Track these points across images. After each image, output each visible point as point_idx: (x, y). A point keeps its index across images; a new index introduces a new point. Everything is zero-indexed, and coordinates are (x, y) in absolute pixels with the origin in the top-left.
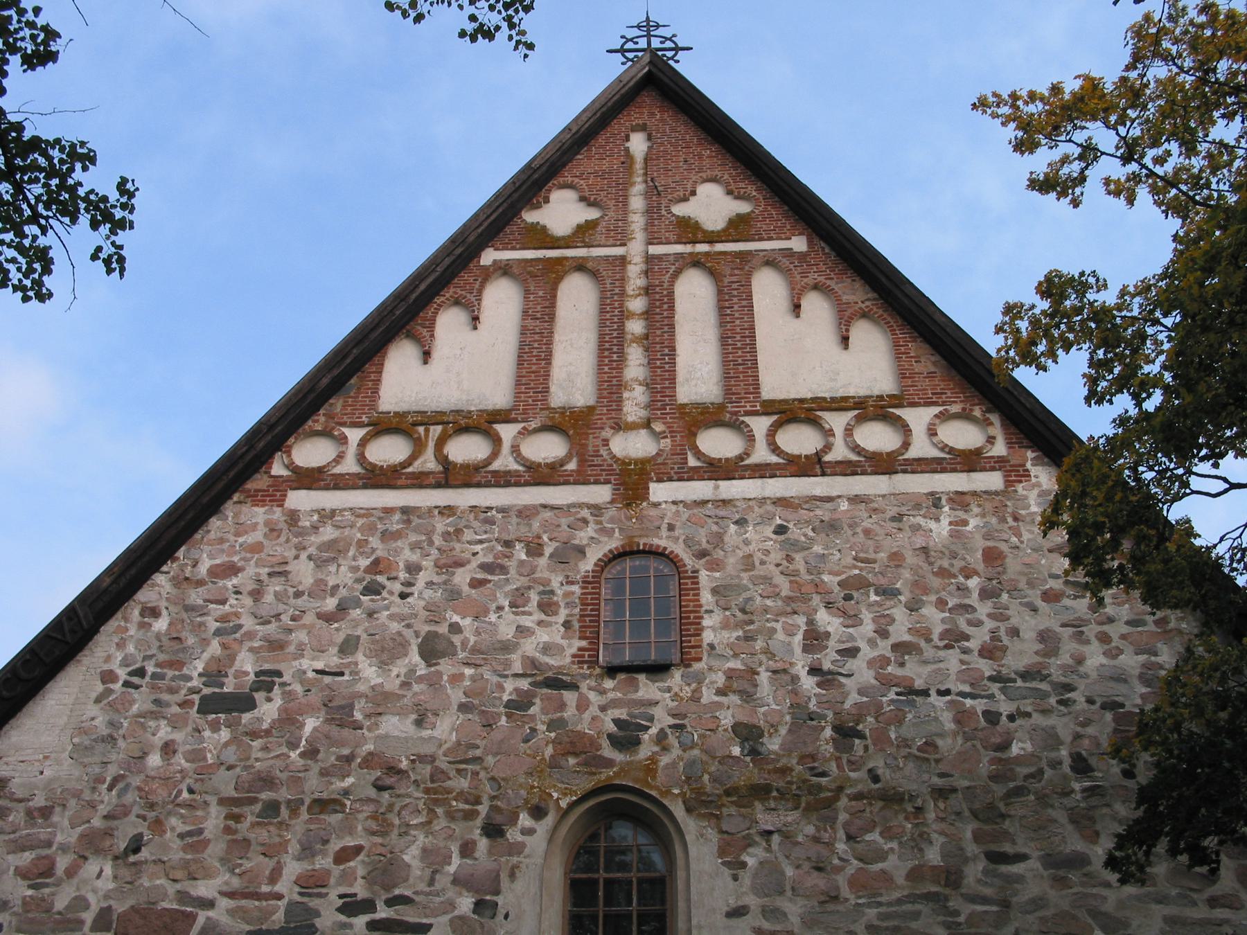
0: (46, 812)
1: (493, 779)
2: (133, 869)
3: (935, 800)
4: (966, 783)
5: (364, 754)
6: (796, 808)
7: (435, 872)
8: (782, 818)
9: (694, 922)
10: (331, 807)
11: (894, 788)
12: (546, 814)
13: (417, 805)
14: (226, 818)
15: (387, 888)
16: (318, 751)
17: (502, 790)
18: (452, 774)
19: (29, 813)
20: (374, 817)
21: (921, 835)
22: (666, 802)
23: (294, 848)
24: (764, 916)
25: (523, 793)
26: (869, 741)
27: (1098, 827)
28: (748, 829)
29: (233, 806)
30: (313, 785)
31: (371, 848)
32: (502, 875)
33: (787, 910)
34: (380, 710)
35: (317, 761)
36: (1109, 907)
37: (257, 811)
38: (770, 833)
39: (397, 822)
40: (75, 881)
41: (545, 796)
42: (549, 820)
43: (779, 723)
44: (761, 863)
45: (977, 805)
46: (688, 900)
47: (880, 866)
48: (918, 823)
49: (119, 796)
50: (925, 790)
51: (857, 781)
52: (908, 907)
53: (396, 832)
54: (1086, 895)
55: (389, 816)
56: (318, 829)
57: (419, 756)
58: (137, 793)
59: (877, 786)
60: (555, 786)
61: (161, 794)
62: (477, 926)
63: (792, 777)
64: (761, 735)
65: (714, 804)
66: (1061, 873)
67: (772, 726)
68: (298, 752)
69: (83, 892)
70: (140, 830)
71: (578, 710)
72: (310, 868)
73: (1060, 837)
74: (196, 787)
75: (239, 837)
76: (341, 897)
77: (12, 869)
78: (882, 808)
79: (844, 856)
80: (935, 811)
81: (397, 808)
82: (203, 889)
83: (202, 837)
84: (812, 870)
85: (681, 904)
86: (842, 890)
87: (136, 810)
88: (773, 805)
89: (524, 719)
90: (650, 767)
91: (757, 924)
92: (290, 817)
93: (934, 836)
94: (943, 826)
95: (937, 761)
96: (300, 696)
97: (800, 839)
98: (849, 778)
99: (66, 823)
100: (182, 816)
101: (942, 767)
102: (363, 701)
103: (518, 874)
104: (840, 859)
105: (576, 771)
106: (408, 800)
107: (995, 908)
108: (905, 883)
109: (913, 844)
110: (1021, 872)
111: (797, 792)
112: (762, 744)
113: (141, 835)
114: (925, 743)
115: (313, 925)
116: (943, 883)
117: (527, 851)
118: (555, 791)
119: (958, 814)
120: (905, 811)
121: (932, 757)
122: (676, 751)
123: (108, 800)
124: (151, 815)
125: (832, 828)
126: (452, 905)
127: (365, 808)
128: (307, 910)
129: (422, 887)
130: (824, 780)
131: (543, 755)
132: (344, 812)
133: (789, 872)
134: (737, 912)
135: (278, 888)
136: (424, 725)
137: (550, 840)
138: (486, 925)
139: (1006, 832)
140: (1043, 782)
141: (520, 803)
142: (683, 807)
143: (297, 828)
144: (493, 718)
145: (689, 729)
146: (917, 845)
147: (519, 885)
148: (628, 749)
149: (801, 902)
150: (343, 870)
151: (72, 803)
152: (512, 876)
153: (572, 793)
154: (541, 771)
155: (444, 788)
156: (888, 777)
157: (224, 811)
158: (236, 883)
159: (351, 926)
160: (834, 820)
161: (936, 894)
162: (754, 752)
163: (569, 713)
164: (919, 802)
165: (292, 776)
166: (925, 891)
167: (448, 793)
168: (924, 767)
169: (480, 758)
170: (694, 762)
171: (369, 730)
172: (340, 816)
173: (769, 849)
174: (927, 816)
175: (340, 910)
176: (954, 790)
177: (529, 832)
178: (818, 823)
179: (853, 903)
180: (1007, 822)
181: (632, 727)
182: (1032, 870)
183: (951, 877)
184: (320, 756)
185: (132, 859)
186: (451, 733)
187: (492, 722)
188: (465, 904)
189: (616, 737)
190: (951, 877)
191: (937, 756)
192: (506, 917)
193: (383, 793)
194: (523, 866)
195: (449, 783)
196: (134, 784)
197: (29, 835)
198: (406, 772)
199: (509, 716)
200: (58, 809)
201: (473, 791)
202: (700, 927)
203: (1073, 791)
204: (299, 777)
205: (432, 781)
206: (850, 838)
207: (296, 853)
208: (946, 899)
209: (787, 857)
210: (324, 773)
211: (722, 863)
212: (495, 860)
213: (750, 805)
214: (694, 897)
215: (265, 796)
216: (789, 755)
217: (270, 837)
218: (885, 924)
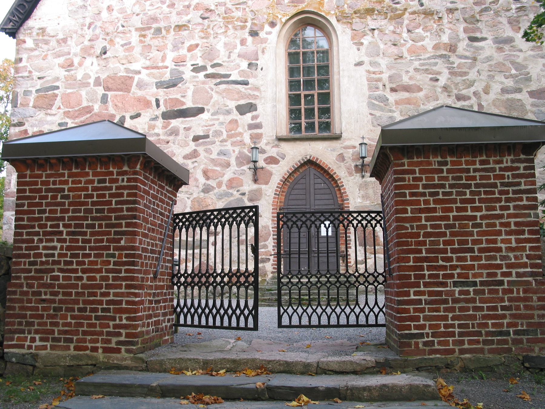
0: (65, 40)
1: (252, 11)
2: (105, 61)
3: (448, 14)
4: (463, 6)
6: (386, 18)
9: (341, 68)
10: (183, 28)
12: (276, 25)
14: (140, 36)
15: (211, 60)
16: (175, 4)
18: (234, 10)
19: (58, 41)
20: (202, 31)
21: (440, 30)
23: (170, 46)
25: (266, 16)
27: (520, 25)
29: (142, 31)
30: (175, 20)
32: (259, 52)
33: (380, 63)
36: (519, 60)
37: (152, 32)
38: (374, 30)
39: (212, 32)
40: (83, 67)
41: (275, 17)
42: (278, 27)
44: (370, 43)
45: (467, 16)
47: (421, 43)
49: (93, 31)
50: (444, 10)
51: (413, 6)
52: (433, 61)
53: (212, 36)
54: (510, 55)
55: (208, 30)
57: (219, 3)
58: (100, 29)
60: (279, 13)
61: (110, 29)
66: (501, 46)
69: (87, 72)
70: (105, 45)
73: (502, 30)
74: (125, 24)
75: (146, 44)
76: (192, 65)
77: (57, 64)
78: (424, 18)
79: (406, 39)
82: (135, 66)
83: (131, 45)
85: (335, 61)
87: (102, 36)
88: (375, 18)
91: (367, 69)
93: (446, 30)
94: (451, 25)
97: (387, 32)
99: (74, 44)
100: (121, 37)
104: (404, 40)
106: (216, 23)
107: (470, 61)
108: (432, 50)
110: (483, 45)
111: (386, 11)
113: (106, 47)
115: (182, 78)
116: (448, 50)
117: (269, 41)
119: (458, 20)
120: (434, 19)
123: (89, 33)
124: (108, 38)
125: (401, 27)
126: (239, 66)
127: (198, 27)
129: (226, 59)
130: (398, 6)
133: (382, 46)
135: (166, 64)
137: (279, 36)
139: (479, 28)
140: (498, 5)
141: (265, 20)
142: (336, 19)
143: (170, 38)
147: (266, 56)
149: (387, 59)
151: (74, 36)
152: (263, 52)
153: (287, 15)
154: (273, 6)
156: (427, 4)
157: (138, 33)
158: (148, 63)
159: (198, 77)
160: (402, 23)
161: (445, 55)
164: (440, 15)
167: (233, 18)
172: (187, 32)
173: (373, 37)
174: (444, 21)
176: (457, 9)
177: (270, 33)
180: (479, 24)
182: (488, 44)
183: (452, 48)
184: (176, 6)
185: (104, 56)
188: (244, 65)
190: (452, 48)
192: (262, 69)
194: (267, 48)
195: (233, 14)
196: (98, 26)
197: (60, 50)
200: (69, 39)
203: (511, 9)
205: (226, 14)
206: (409, 31)
208: (449, 57)
210: (178, 14)
213: (366, 18)
214: (341, 58)
215: (155, 26)
217: (159, 43)
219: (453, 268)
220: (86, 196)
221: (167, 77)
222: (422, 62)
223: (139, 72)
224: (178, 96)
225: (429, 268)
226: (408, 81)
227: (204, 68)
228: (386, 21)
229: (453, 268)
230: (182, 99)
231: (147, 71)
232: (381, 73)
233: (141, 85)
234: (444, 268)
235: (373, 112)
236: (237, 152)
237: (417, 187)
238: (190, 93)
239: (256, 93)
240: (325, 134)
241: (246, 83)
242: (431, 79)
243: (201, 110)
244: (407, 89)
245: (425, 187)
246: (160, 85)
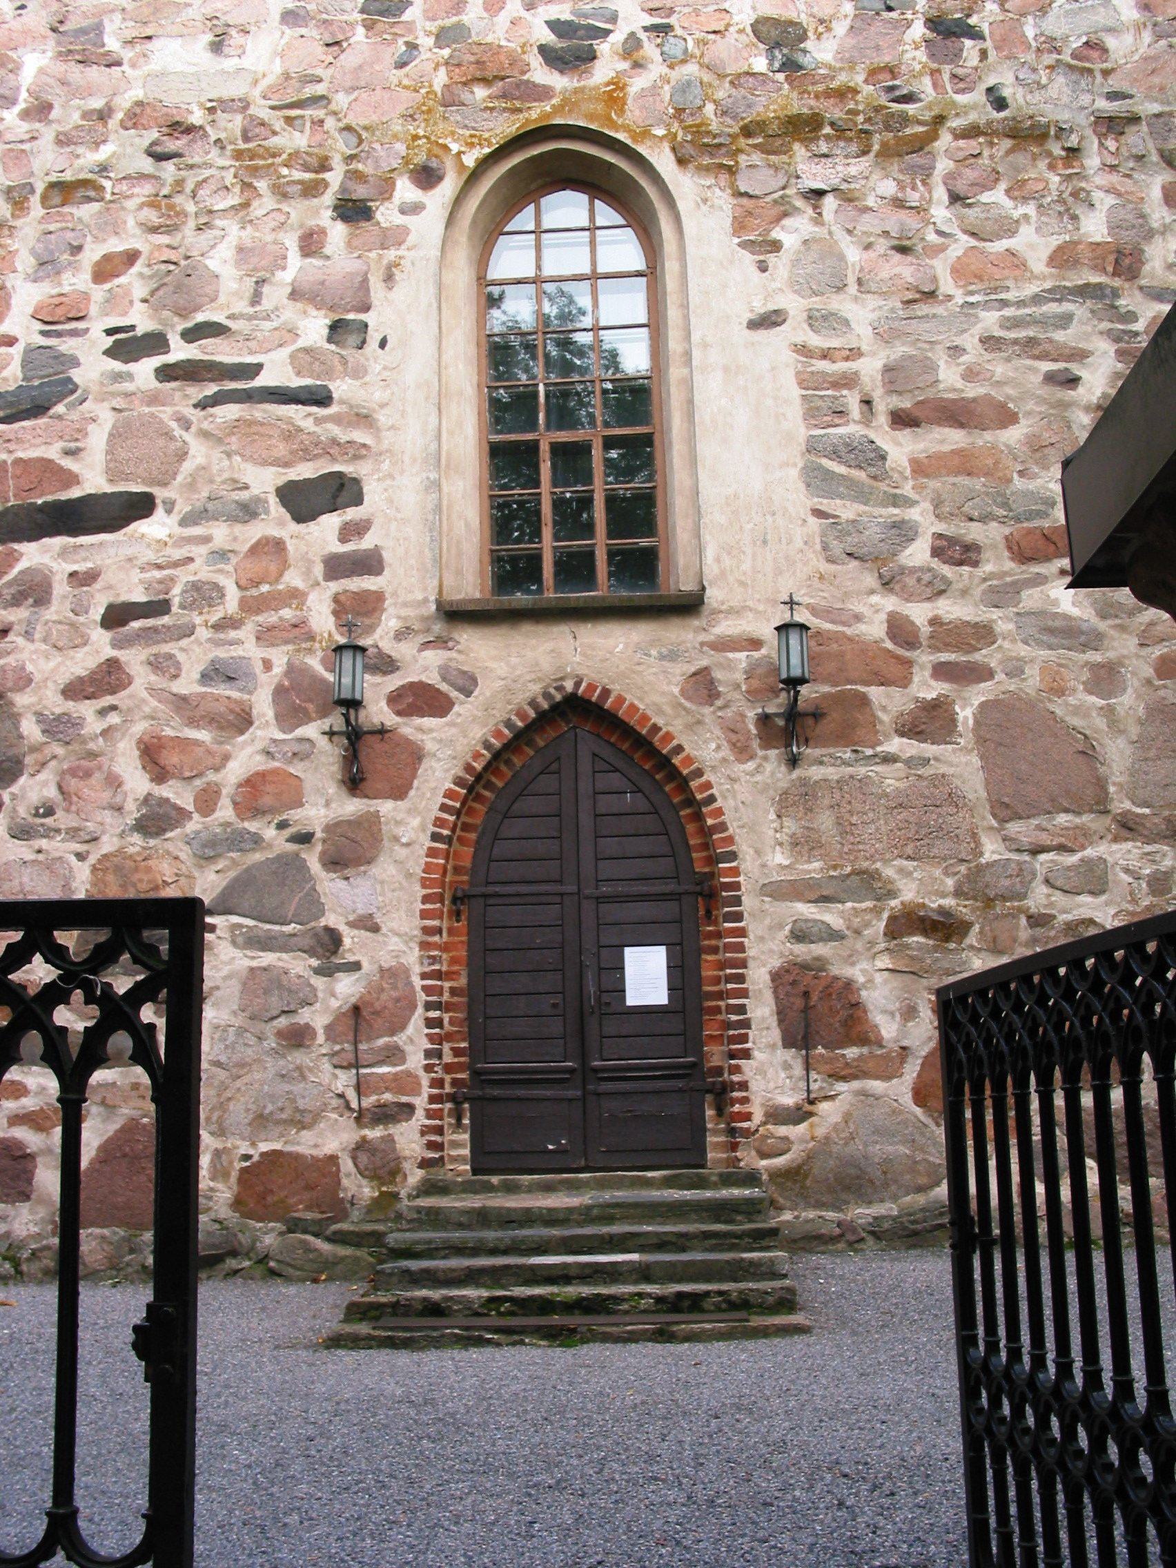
1: (348, 128)
3: (1101, 137)
4: (1156, 108)
5: (127, 105)
6: (865, 153)
7: (261, 282)
8: (839, 168)
9: (696, 337)
10: (81, 192)
11: (1031, 117)
12: (440, 179)
13: (223, 178)
15: (183, 313)
16: (50, 107)
17: (365, 146)
18: (278, 125)
20: (153, 204)
21: (1075, 195)
22: (641, 149)
24: (810, 325)
25: (400, 148)
26: (988, 44)
28: (784, 188)
31: (151, 253)
33: (849, 316)
34: (149, 32)
35: (51, 122)
38: (820, 193)
39: (191, 208)
41: (436, 150)
42: (448, 187)
43: (833, 17)
44: (805, 242)
46: (685, 306)
48: (1070, 176)
50: (1084, 120)
51: (966, 109)
52: (1052, 308)
53: (192, 223)
55: (178, 199)
56: (62, 229)
59: (1002, 114)
60: (453, 133)
62: (336, 360)
63: (857, 103)
64: (803, 37)
65: (724, 150)
67: (822, 21)
68: (17, 109)
71: (486, 10)
72: (55, 291)
76: (110, 332)
78: (1009, 152)
80: (1100, 153)
81: (189, 186)
84: (893, 252)
86: (941, 282)
89: (394, 30)
90: (614, 96)
92: (13, 215)
93: (1097, 195)
94: (1114, 178)
95: (1106, 73)
96: (9, 17)
97: (871, 202)
98: (954, 104)
101: (1114, 83)
102: (118, 17)
103: (398, 276)
104: (940, 233)
105: (487, 108)
106: (207, 173)
109: (1062, 209)
111: (866, 127)
112: (805, 51)
114: (1086, 43)
115: (70, 380)
116: (1110, 269)
117: (411, 239)
118: (455, 141)
119: (1140, 158)
120: (1049, 154)
121: (1098, 67)
122: (657, 69)
125: (924, 182)
126: (293, 332)
127: (136, 190)
128: (56, 358)
129: (242, 306)
130: (910, 108)
131: (431, 86)
132: (102, 199)
133: (853, 255)
134: (768, 321)
136: (226, 50)
137: (451, 221)
138: (351, 359)
143: (27, 230)
144: (343, 31)
145: (679, 32)
146: (1068, 210)
147: (401, 292)
148: (577, 67)
149: (873, 301)
150: (109, 291)
152: (389, 278)
154: (429, 111)
155: (267, 149)
156: (1021, 101)
159: (130, 377)
161: (1099, 286)
162: (791, 66)
163: (472, 15)
164: (1073, 141)
165: (11, 150)
166: (1080, 282)
168: (1083, 84)
169: (323, 97)
170: (689, 83)
171: (133, 65)
172: (96, 206)
173: (818, 219)
175: (110, 353)
176: (1135, 119)
177: (414, 209)
178: (901, 177)
179: (961, 302)
181: (581, 33)
184: (54, 114)
186: (272, 62)
187: (340, 37)
188: (314, 328)
189: (553, 50)
191: (1105, 65)
192: (383, 344)
193: (164, 163)
195: (274, 141)
198: (201, 127)
199: (369, 26)
201: (316, 150)
202: (705, 346)
204: (23, 151)
205: (246, 139)
206: (956, 198)
207: (30, 271)
208: (1116, 294)
209: (849, 232)
211: (739, 245)
212: (359, 257)
213: (787, 151)
216: (852, 69)
218: (1012, 335)
222: (1009, 312)
224: (53, 452)
227: (156, 342)
230: (67, 463)
232: (854, 354)
235: (825, 504)
236: (278, 670)
238: (97, 440)
239: (359, 436)
241: (320, 398)
242: (1050, 378)
243: (141, 506)
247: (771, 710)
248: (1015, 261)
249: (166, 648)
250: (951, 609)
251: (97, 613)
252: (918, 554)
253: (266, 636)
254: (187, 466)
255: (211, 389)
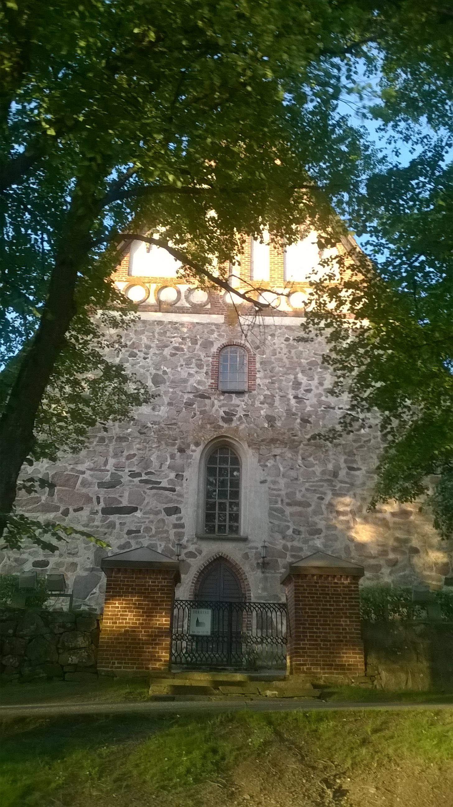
23: (111, 453)
42: (201, 448)
82: (80, 467)
90: (236, 430)
134: (263, 482)
135: (108, 467)
149: (285, 479)
162: (272, 426)
173: (275, 461)
183: (335, 474)
188: (172, 475)
208: (333, 481)
219: (321, 633)
220: (145, 589)
221: (107, 478)
222: (311, 484)
223: (84, 473)
224: (117, 496)
225: (310, 632)
226: (300, 498)
227: (139, 475)
228: (287, 449)
229: (321, 633)
230: (119, 499)
231: (92, 473)
232: (280, 490)
233: (85, 484)
234: (316, 633)
235: (272, 521)
236: (162, 547)
237: (304, 593)
238: (126, 494)
239: (180, 499)
240: (234, 536)
241: (173, 490)
242: (319, 498)
243: (135, 509)
244: (299, 504)
245: (308, 593)
246: (101, 485)
247: (259, 561)
248: (314, 473)
249: (139, 540)
250: (296, 543)
251: (125, 531)
252: (290, 532)
253: (161, 539)
254: (146, 502)
255: (151, 486)
